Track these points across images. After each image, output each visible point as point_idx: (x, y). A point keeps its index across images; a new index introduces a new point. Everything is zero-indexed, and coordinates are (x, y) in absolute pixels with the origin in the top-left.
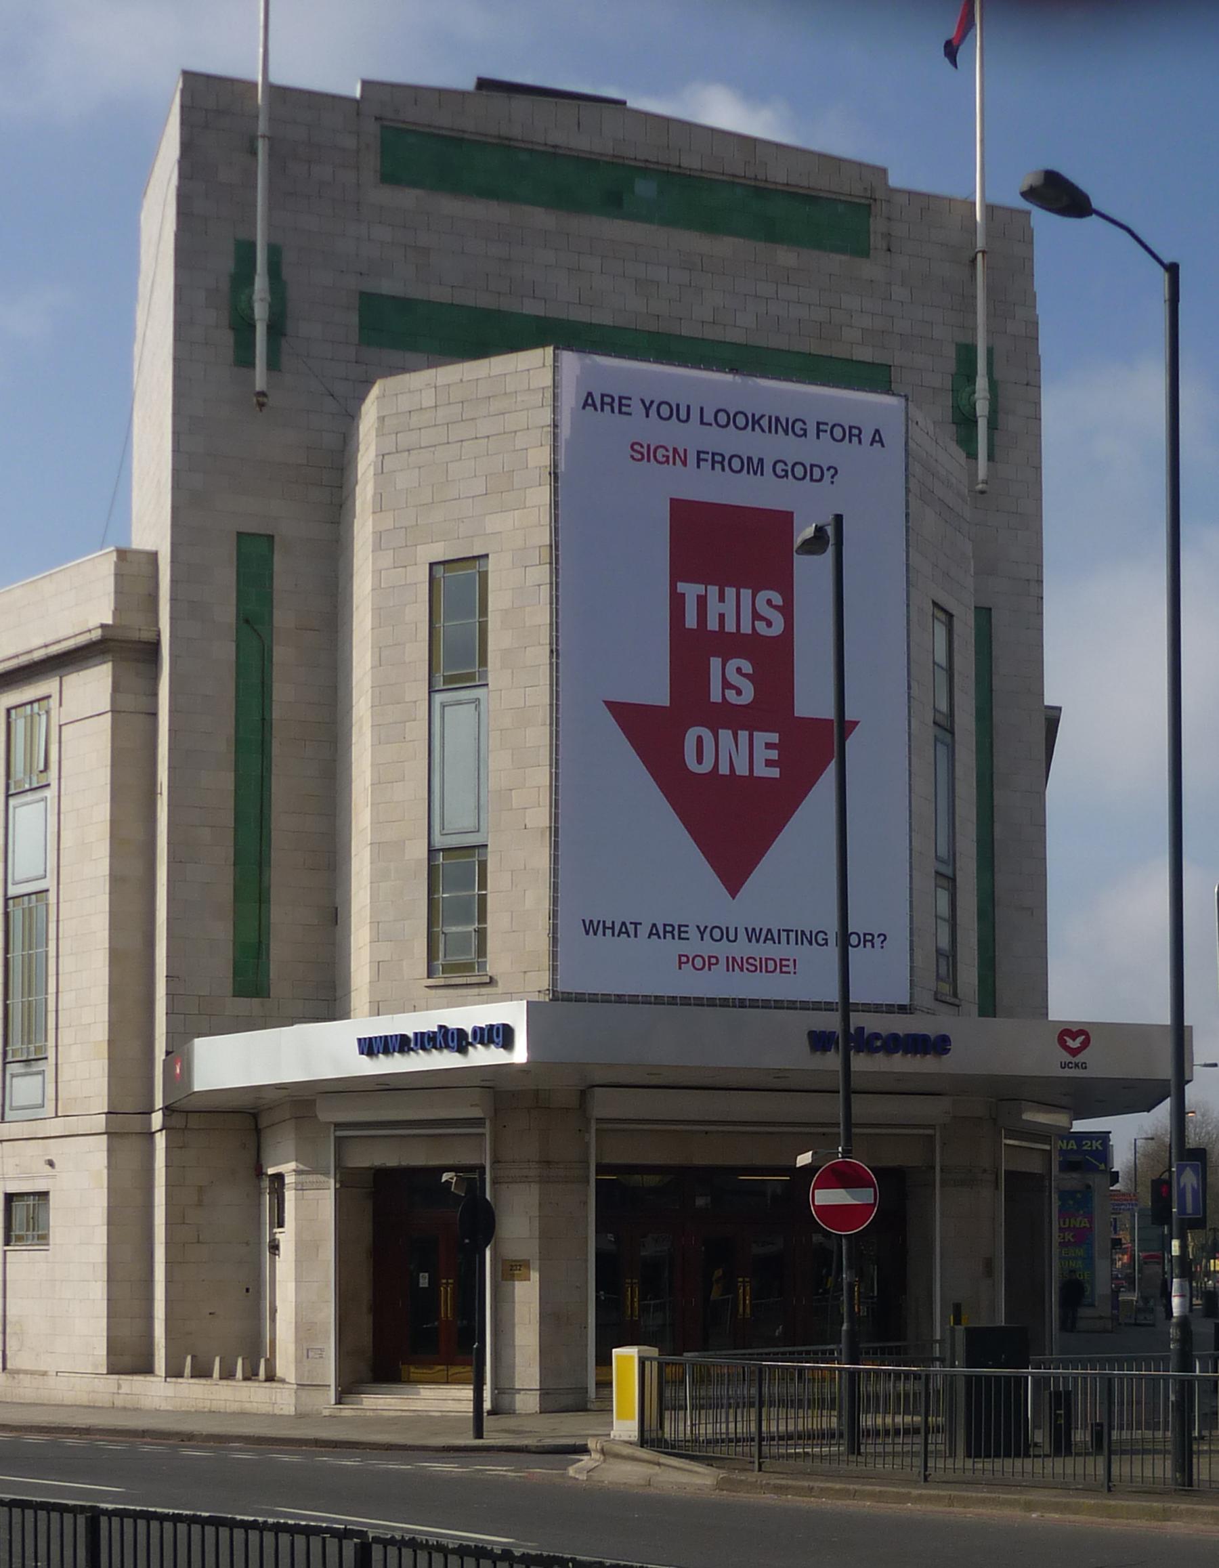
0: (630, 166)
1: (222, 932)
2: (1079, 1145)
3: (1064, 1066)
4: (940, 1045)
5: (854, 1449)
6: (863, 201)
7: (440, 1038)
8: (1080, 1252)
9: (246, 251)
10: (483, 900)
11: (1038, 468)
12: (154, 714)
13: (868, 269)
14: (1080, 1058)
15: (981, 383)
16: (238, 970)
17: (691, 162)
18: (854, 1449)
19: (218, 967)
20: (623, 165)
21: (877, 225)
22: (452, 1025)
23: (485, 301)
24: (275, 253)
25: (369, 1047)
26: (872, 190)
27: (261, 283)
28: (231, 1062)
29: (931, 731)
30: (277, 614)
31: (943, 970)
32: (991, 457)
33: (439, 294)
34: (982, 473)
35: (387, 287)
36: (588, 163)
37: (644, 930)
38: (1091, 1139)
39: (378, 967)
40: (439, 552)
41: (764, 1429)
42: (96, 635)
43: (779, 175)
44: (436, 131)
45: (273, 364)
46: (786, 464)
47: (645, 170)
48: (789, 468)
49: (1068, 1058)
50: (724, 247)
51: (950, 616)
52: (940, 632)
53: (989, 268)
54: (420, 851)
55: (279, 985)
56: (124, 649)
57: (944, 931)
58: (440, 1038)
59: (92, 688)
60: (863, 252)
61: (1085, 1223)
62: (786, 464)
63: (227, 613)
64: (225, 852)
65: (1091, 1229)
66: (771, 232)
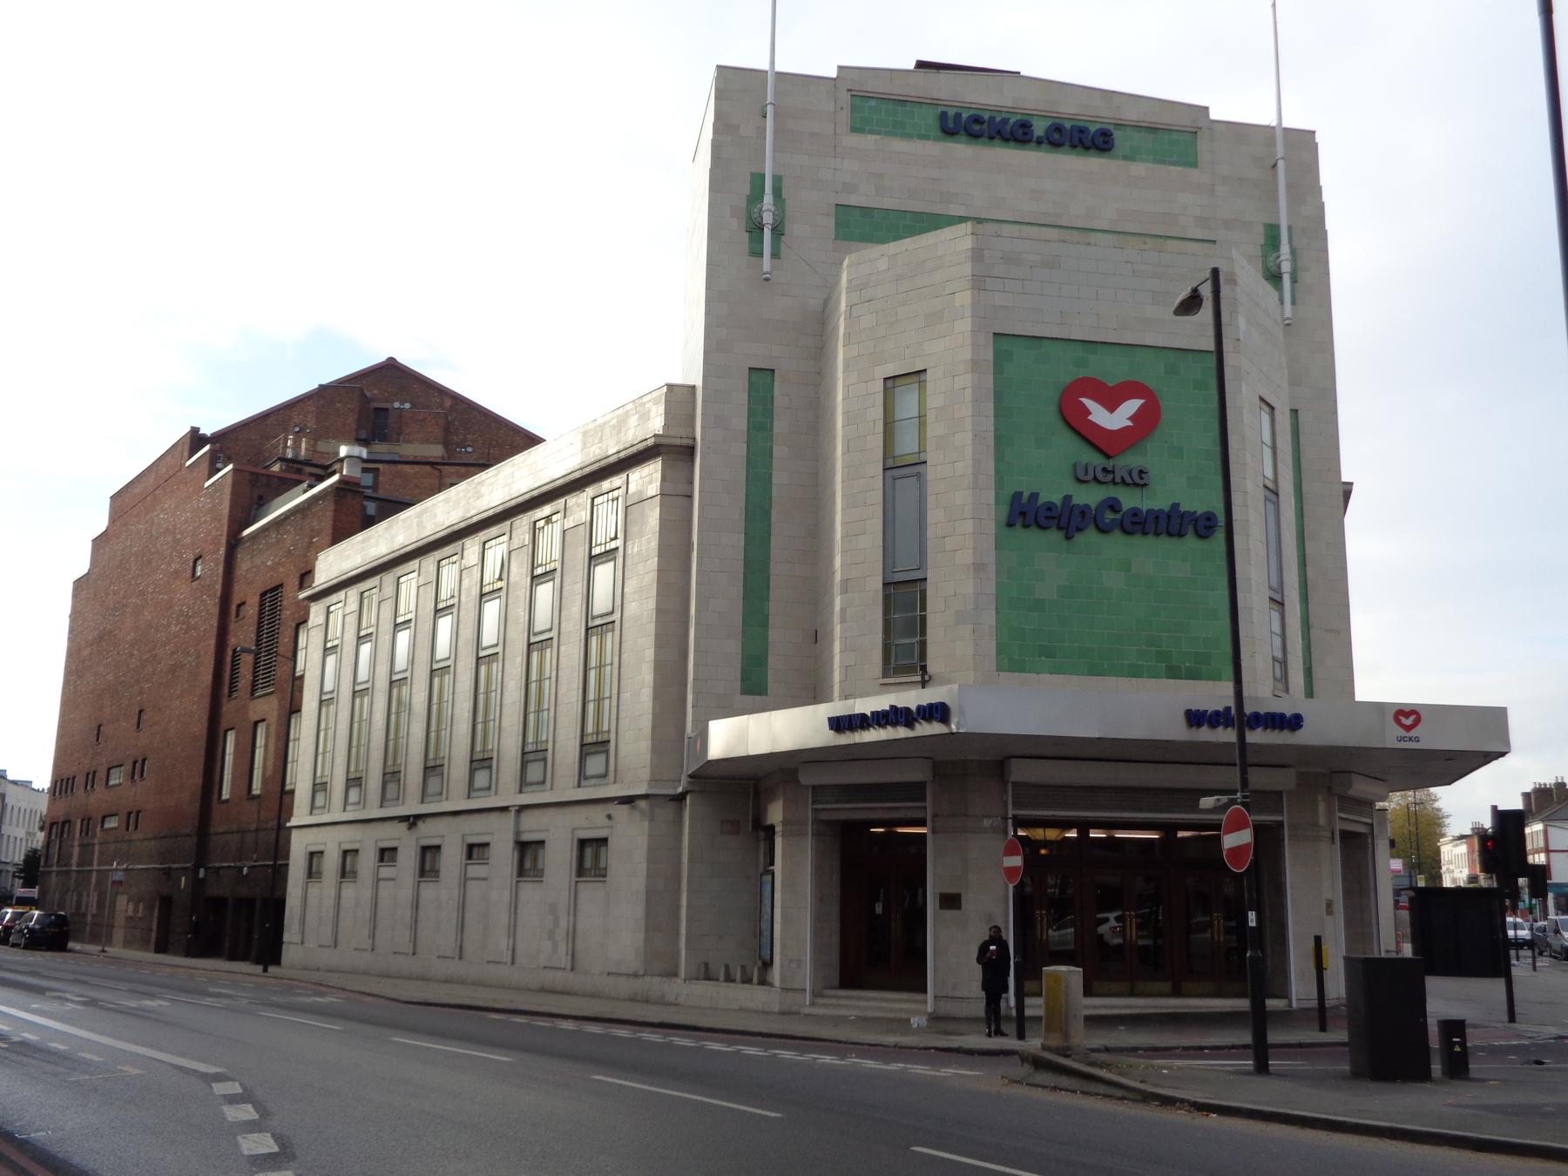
1: (734, 648)
3: (1401, 739)
4: (1295, 723)
5: (1262, 1068)
7: (891, 716)
9: (758, 180)
10: (923, 619)
12: (690, 497)
13: (1195, 175)
14: (1413, 733)
15: (1285, 249)
16: (745, 678)
18: (1262, 1068)
19: (732, 674)
21: (1203, 145)
22: (900, 705)
24: (777, 180)
25: (838, 724)
27: (768, 199)
28: (728, 737)
29: (1261, 493)
30: (776, 423)
31: (1278, 674)
32: (1293, 303)
33: (888, 203)
34: (1288, 314)
35: (854, 200)
39: (846, 668)
40: (892, 369)
42: (650, 442)
45: (775, 255)
49: (1402, 733)
51: (1272, 408)
52: (1266, 418)
53: (1287, 169)
54: (876, 584)
55: (772, 686)
56: (672, 451)
57: (1277, 641)
58: (891, 716)
59: (647, 479)
63: (740, 423)
64: (737, 590)
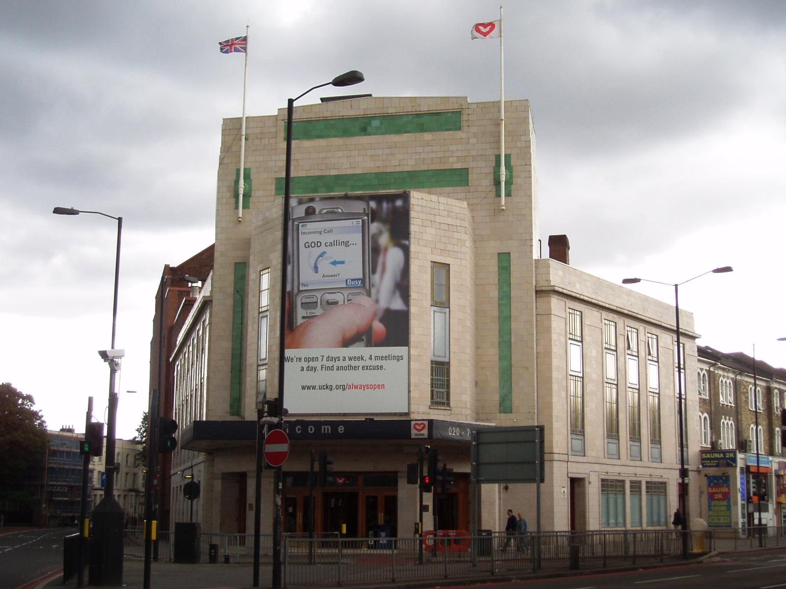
0: (369, 117)
2: (724, 455)
6: (458, 110)
8: (725, 503)
11: (530, 196)
13: (458, 134)
17: (391, 111)
20: (367, 117)
21: (464, 117)
23: (318, 173)
26: (461, 105)
36: (355, 119)
37: (317, 387)
38: (729, 452)
41: (444, 566)
43: (424, 108)
44: (303, 120)
46: (309, 243)
47: (374, 118)
48: (310, 244)
50: (405, 137)
60: (459, 129)
61: (726, 490)
62: (309, 243)
65: (729, 493)
66: (422, 129)
